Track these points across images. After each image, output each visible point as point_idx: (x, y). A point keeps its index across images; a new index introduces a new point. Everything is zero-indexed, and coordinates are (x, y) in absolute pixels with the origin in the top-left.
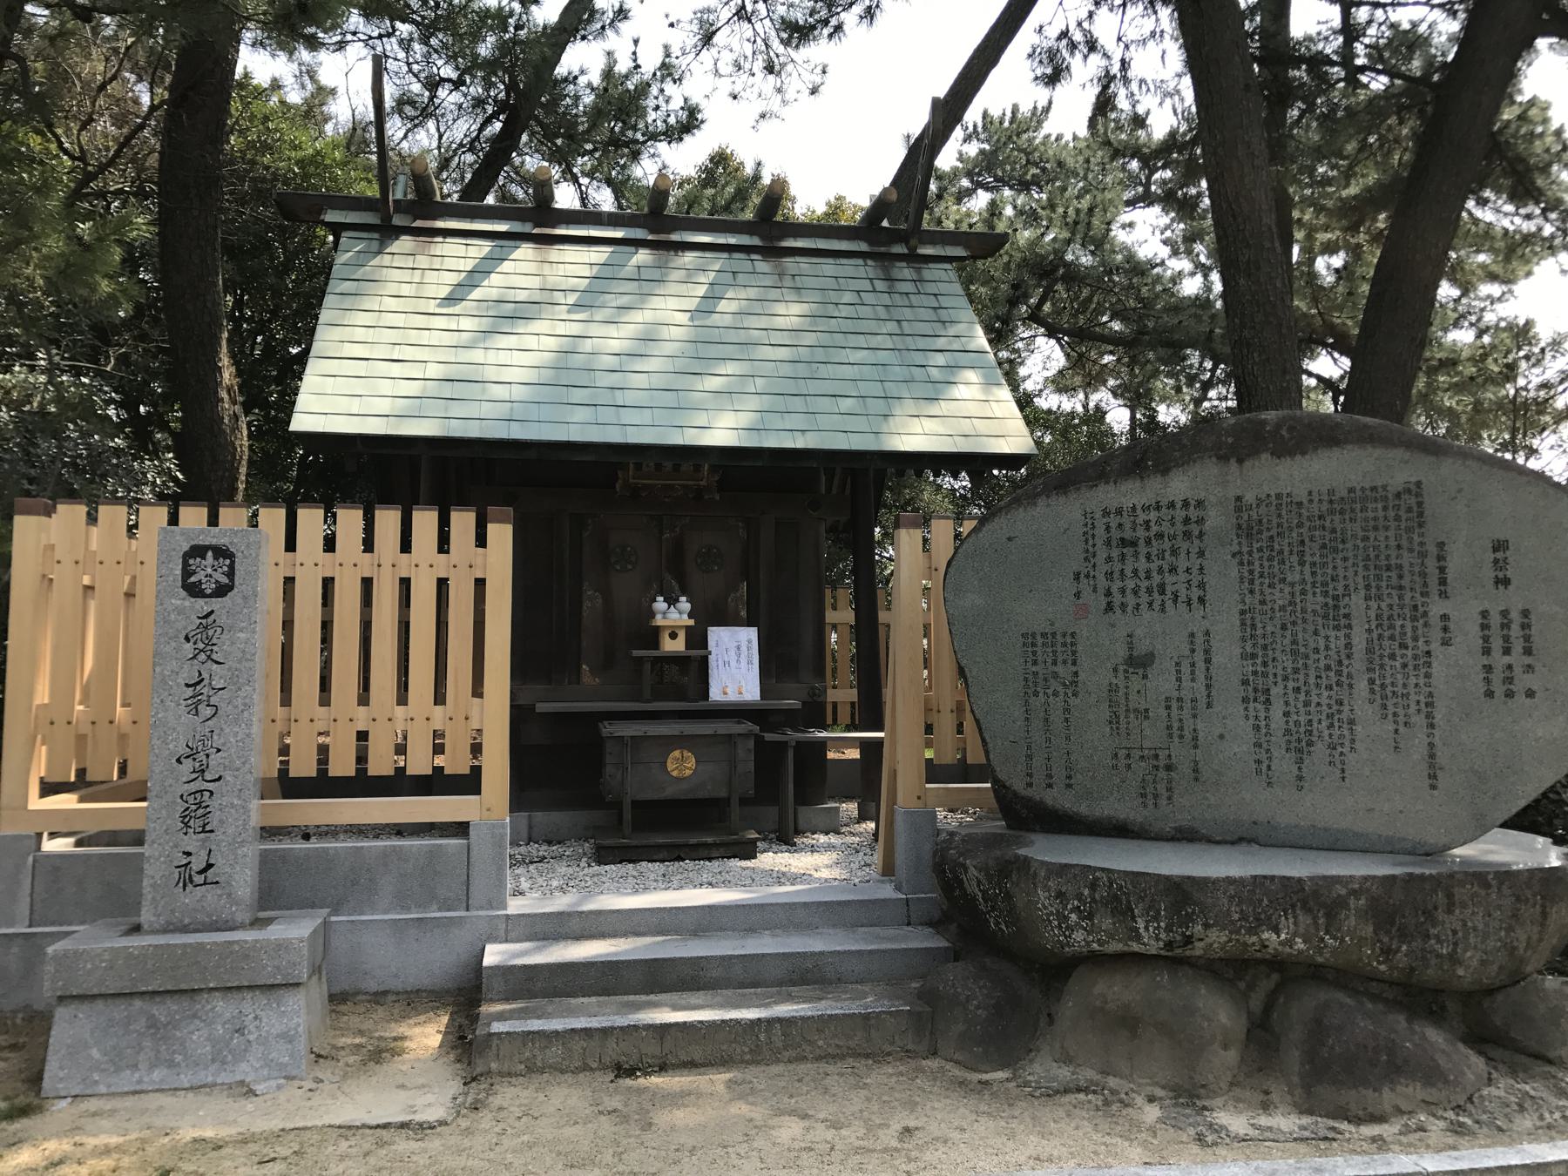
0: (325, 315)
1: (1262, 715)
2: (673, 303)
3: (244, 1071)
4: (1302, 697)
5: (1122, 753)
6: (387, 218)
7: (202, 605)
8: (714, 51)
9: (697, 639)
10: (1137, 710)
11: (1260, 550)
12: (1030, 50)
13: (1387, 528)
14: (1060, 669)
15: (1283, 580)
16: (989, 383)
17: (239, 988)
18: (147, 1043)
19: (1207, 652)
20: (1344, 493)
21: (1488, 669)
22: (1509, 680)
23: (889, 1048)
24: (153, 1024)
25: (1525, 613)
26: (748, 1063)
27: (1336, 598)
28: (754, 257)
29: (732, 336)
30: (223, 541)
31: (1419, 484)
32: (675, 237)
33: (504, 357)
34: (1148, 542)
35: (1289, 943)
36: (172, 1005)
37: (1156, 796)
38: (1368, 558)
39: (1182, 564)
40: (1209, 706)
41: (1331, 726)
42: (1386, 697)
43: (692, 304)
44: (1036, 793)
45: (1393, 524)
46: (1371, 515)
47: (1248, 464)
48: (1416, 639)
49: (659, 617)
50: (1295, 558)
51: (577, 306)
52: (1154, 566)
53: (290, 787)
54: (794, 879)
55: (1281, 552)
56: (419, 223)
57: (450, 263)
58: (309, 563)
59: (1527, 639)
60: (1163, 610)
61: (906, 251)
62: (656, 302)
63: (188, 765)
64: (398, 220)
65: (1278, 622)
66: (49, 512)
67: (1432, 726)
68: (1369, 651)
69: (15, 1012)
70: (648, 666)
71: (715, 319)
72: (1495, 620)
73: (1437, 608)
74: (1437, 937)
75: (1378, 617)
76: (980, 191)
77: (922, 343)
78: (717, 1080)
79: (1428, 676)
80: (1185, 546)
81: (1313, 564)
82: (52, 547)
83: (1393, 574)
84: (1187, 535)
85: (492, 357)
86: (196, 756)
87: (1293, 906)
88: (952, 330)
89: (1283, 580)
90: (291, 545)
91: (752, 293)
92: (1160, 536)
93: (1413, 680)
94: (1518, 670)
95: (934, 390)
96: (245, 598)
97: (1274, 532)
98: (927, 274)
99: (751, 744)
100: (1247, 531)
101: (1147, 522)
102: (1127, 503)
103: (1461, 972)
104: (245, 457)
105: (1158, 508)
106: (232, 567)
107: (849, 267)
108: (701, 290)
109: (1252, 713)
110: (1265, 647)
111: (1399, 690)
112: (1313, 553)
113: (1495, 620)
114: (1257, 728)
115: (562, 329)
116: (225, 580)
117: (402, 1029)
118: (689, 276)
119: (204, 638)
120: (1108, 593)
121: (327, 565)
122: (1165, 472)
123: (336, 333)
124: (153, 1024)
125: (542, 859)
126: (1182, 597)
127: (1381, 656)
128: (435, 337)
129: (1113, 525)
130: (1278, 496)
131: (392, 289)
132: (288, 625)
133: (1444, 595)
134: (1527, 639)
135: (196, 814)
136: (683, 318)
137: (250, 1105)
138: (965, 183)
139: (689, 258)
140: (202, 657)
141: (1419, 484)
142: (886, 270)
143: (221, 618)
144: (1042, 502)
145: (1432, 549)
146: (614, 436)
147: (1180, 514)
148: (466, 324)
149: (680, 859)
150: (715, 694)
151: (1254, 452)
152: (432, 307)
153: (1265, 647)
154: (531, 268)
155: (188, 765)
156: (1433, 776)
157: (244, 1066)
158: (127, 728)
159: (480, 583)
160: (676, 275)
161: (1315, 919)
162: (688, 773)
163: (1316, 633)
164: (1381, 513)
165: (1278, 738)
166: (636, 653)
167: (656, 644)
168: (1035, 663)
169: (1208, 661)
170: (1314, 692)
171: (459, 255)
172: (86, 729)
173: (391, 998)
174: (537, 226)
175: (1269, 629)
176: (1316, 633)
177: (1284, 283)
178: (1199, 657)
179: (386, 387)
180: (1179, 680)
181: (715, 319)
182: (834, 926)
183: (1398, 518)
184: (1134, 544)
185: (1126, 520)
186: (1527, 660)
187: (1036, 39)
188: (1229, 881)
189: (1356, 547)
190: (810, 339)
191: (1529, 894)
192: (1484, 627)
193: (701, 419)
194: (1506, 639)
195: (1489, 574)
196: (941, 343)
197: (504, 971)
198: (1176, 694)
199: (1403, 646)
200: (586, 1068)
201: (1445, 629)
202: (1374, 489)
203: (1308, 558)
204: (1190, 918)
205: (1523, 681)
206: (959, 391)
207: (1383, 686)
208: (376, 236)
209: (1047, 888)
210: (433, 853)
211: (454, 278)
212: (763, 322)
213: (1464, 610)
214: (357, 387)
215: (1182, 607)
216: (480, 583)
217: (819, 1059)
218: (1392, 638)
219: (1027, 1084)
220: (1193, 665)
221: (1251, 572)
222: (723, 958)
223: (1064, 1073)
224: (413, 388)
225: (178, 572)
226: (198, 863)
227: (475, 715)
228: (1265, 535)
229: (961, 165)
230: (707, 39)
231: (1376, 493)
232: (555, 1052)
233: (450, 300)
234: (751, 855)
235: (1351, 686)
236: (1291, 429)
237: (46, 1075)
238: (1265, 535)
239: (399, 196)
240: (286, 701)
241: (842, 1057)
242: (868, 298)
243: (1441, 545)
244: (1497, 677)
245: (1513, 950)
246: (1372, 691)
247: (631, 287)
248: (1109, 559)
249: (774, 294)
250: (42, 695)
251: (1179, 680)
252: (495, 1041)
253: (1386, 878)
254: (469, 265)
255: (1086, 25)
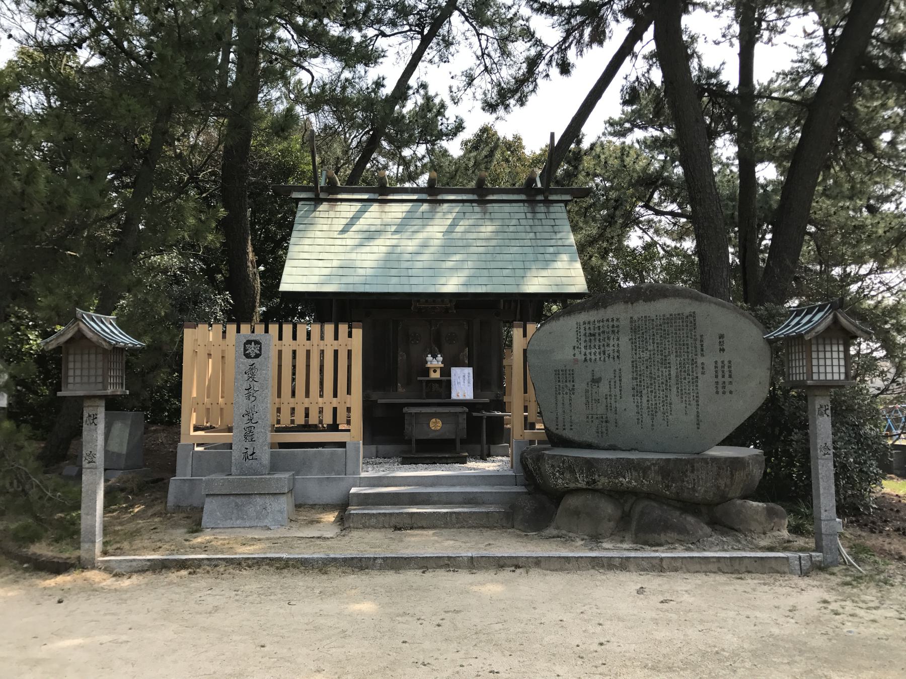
0: (293, 240)
1: (639, 401)
2: (436, 228)
3: (267, 522)
4: (653, 394)
5: (590, 416)
6: (317, 195)
7: (250, 361)
8: (473, 89)
9: (446, 372)
10: (595, 400)
11: (639, 338)
12: (621, 88)
13: (683, 330)
14: (568, 384)
15: (647, 350)
16: (572, 260)
17: (264, 494)
18: (235, 511)
19: (620, 377)
20: (668, 316)
21: (717, 383)
22: (724, 387)
23: (495, 525)
24: (237, 505)
25: (730, 362)
26: (443, 528)
27: (665, 356)
28: (474, 205)
29: (460, 243)
30: (257, 338)
31: (694, 313)
32: (440, 197)
33: (364, 257)
34: (599, 335)
35: (630, 482)
36: (243, 499)
37: (602, 433)
38: (676, 341)
39: (611, 343)
40: (621, 398)
41: (663, 405)
42: (682, 394)
43: (444, 229)
44: (560, 432)
45: (685, 328)
46: (678, 324)
47: (634, 305)
48: (693, 372)
49: (429, 363)
50: (651, 341)
51: (396, 232)
52: (601, 344)
53: (278, 430)
54: (474, 469)
55: (646, 338)
56: (331, 197)
57: (344, 215)
58: (287, 345)
59: (730, 371)
60: (604, 360)
61: (543, 198)
62: (429, 229)
63: (246, 417)
64: (322, 196)
65: (645, 365)
66: (195, 327)
67: (698, 405)
68: (677, 376)
69: (187, 507)
70: (424, 384)
71: (454, 235)
72: (720, 364)
73: (700, 360)
74: (687, 481)
75: (680, 363)
76: (636, 130)
77: (544, 243)
78: (431, 532)
79: (697, 386)
80: (612, 336)
81: (658, 343)
82: (197, 340)
83: (685, 347)
84: (613, 332)
85: (359, 257)
86: (249, 415)
87: (630, 469)
88: (559, 236)
89: (647, 350)
90: (280, 338)
91: (471, 222)
92: (604, 332)
93: (692, 387)
94: (727, 383)
95: (547, 263)
96: (265, 359)
97: (644, 331)
98: (552, 209)
99: (465, 416)
100: (634, 330)
101: (599, 327)
102: (592, 319)
103: (697, 495)
104: (259, 292)
105: (603, 321)
106: (260, 348)
107: (516, 207)
108: (449, 222)
109: (636, 401)
110: (640, 375)
111: (687, 392)
112: (658, 339)
113: (720, 364)
114: (637, 406)
115: (389, 243)
116: (258, 352)
117: (321, 516)
118: (444, 215)
119: (251, 373)
120: (585, 355)
121: (294, 345)
122: (605, 307)
123: (297, 248)
124: (237, 505)
125: (381, 463)
126: (611, 356)
127: (681, 379)
128: (337, 249)
129: (587, 328)
130: (645, 317)
131: (319, 227)
132: (280, 366)
133: (702, 355)
134: (730, 371)
135: (249, 435)
136: (440, 235)
137: (269, 532)
138: (627, 125)
139: (445, 206)
140: (251, 379)
141: (694, 313)
142: (533, 209)
143: (257, 366)
144: (561, 318)
145: (698, 337)
146: (407, 290)
147: (611, 324)
148: (349, 242)
149: (435, 463)
150: (454, 396)
151: (637, 300)
152: (336, 235)
153: (640, 375)
154: (377, 215)
155: (246, 417)
156: (698, 424)
157: (266, 521)
158: (223, 406)
159: (350, 352)
160: (439, 215)
161: (639, 473)
162: (439, 428)
163: (658, 370)
164: (681, 324)
165: (645, 410)
166: (419, 378)
167: (428, 375)
168: (559, 381)
169: (620, 380)
170: (658, 392)
171: (347, 210)
172: (209, 406)
173: (318, 507)
174: (380, 195)
175: (642, 368)
176: (658, 370)
177: (717, 209)
178: (617, 379)
179: (316, 271)
180: (610, 388)
181: (454, 235)
182: (486, 485)
183: (687, 326)
184: (594, 335)
185: (592, 326)
186: (730, 380)
187: (624, 82)
188: (607, 459)
189: (672, 337)
190: (494, 243)
191: (724, 466)
192: (716, 367)
193: (443, 280)
194: (723, 372)
195: (718, 347)
196: (553, 242)
197: (357, 495)
198: (609, 393)
199: (689, 375)
200: (384, 527)
201: (703, 368)
202: (679, 314)
203: (656, 341)
204: (593, 473)
205: (728, 388)
206: (559, 265)
207: (681, 390)
208: (313, 203)
209: (548, 464)
210: (332, 454)
211: (345, 221)
212: (474, 236)
213: (708, 360)
214: (306, 271)
215: (611, 359)
216: (350, 352)
217: (469, 527)
218: (685, 372)
219: (542, 536)
220: (615, 382)
221: (636, 346)
222: (438, 493)
223: (555, 532)
224: (326, 271)
225: (242, 350)
226: (250, 452)
227: (348, 401)
228: (641, 332)
229: (623, 116)
230: (470, 84)
231: (680, 316)
232: (373, 520)
233: (343, 231)
234: (465, 462)
235: (670, 390)
236: (651, 291)
237: (203, 520)
238: (641, 332)
239: (322, 185)
240: (279, 396)
241: (478, 527)
242: (523, 222)
243: (702, 336)
244: (720, 386)
245: (718, 487)
246: (678, 392)
247: (419, 222)
248: (585, 341)
249: (481, 222)
250: (194, 395)
251: (610, 388)
252: (352, 516)
253: (666, 459)
254: (351, 215)
255: (646, 75)
